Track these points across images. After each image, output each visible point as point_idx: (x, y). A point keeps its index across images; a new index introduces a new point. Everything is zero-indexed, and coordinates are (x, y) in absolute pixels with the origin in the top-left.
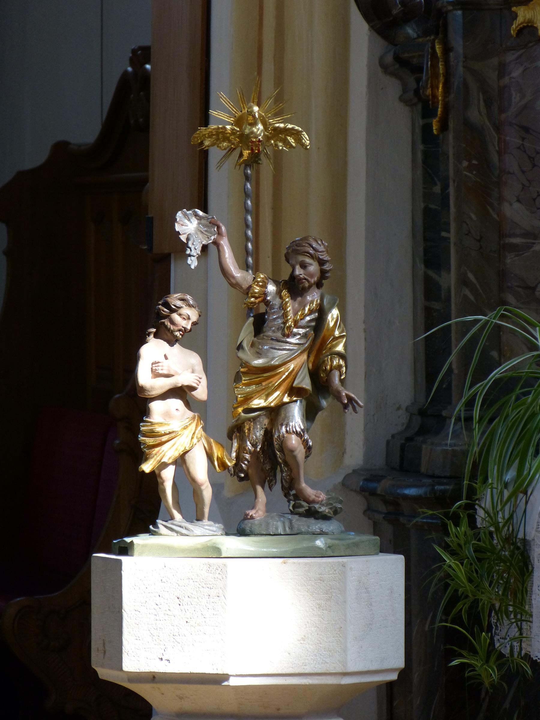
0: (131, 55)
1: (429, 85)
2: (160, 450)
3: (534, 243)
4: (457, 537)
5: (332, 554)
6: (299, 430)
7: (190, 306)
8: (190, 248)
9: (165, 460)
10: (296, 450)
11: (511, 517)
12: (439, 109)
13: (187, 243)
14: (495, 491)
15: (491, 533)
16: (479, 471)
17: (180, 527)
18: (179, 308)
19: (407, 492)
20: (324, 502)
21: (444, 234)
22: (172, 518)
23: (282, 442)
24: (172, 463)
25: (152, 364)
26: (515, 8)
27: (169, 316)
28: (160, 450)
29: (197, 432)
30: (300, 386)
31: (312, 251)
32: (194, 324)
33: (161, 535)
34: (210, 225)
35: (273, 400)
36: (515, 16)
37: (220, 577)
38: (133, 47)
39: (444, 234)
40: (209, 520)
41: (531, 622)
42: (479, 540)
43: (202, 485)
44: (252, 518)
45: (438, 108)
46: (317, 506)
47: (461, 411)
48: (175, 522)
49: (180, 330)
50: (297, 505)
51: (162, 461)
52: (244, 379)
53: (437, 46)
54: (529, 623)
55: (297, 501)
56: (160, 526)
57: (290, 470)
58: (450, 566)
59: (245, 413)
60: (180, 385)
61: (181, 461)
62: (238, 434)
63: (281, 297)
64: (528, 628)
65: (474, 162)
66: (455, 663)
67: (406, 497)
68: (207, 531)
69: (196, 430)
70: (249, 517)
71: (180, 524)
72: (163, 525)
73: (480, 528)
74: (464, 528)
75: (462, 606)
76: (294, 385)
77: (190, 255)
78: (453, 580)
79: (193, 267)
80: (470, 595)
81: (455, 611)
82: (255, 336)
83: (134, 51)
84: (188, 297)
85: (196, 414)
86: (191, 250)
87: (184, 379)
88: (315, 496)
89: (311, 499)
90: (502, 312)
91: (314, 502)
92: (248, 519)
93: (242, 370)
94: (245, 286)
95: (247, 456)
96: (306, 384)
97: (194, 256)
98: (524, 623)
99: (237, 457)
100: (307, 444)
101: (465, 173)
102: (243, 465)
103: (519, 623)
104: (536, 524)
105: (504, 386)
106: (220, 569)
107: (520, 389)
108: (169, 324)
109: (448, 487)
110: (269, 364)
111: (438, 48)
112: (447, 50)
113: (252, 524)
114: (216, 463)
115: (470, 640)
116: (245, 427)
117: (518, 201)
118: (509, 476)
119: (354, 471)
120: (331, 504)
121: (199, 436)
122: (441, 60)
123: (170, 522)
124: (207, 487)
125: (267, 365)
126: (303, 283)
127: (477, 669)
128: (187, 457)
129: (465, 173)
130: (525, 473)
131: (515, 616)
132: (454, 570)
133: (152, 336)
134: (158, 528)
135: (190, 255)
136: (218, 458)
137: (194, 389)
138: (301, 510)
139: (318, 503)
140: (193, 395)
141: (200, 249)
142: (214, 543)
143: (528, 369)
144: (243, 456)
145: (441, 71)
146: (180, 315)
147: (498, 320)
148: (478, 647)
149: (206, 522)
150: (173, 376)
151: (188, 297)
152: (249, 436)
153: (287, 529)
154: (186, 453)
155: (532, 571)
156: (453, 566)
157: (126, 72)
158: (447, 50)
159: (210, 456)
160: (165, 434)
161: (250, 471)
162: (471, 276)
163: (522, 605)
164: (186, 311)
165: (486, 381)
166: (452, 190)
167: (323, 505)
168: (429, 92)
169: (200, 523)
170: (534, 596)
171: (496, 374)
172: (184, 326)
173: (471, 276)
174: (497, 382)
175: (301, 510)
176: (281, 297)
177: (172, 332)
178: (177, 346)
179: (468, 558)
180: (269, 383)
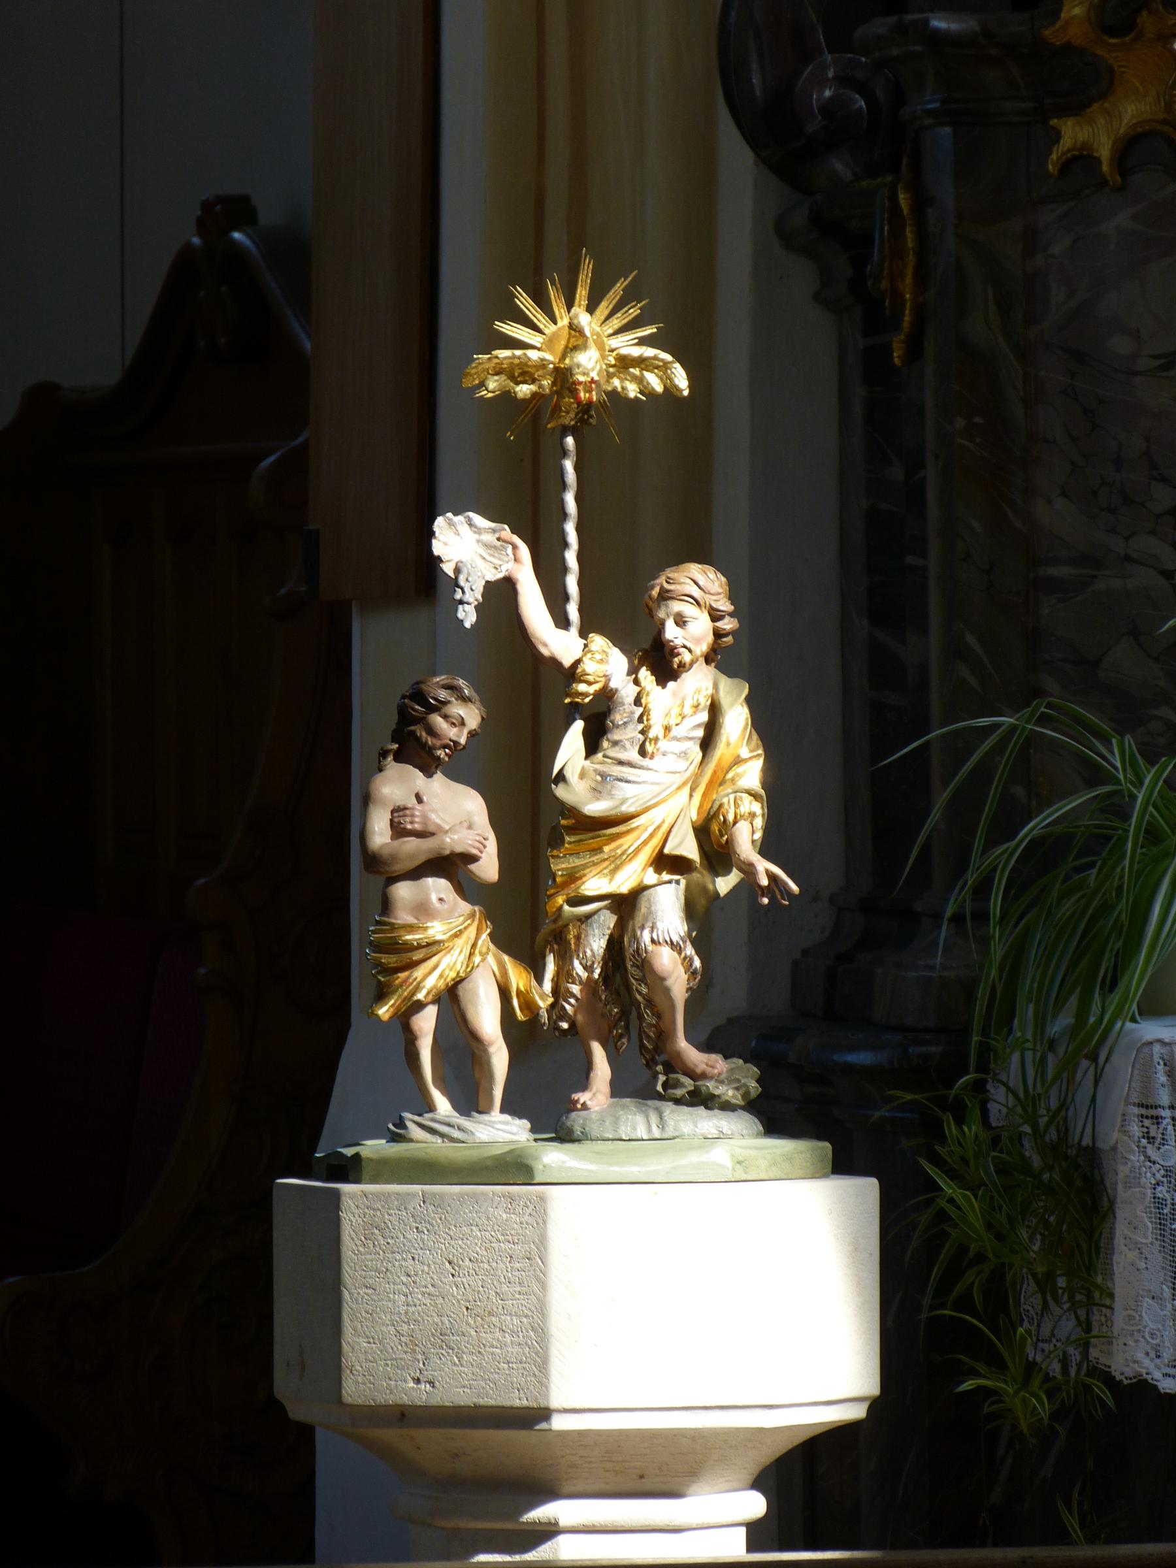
0: (199, 213)
1: (886, 272)
2: (408, 977)
3: (1095, 577)
4: (960, 1144)
5: (744, 1177)
6: (675, 939)
7: (464, 699)
8: (462, 589)
9: (420, 996)
10: (670, 976)
11: (1063, 1105)
12: (907, 318)
13: (457, 578)
14: (1029, 1055)
15: (1021, 1135)
16: (1004, 1015)
17: (449, 1125)
18: (445, 703)
19: (853, 1058)
20: (723, 1076)
21: (910, 559)
22: (430, 1107)
23: (644, 964)
24: (433, 1002)
25: (392, 812)
26: (1055, 121)
27: (424, 718)
28: (408, 977)
29: (480, 942)
30: (677, 852)
31: (696, 592)
32: (472, 735)
33: (411, 1141)
34: (499, 543)
35: (623, 883)
36: (1057, 136)
37: (531, 1220)
38: (204, 198)
39: (910, 559)
40: (502, 1111)
41: (1112, 1309)
42: (1001, 1151)
43: (491, 1044)
44: (585, 1107)
45: (903, 314)
46: (711, 1085)
47: (965, 901)
48: (438, 1117)
49: (445, 747)
50: (671, 1082)
51: (415, 998)
52: (567, 839)
53: (901, 196)
54: (1104, 1309)
55: (671, 1076)
56: (409, 1124)
57: (658, 1016)
58: (951, 1201)
59: (571, 906)
60: (447, 852)
61: (451, 998)
62: (556, 947)
63: (636, 682)
64: (1103, 1319)
65: (978, 420)
66: (967, 1385)
67: (850, 1069)
68: (500, 1133)
69: (477, 939)
70: (579, 1106)
71: (447, 1120)
72: (415, 1122)
73: (997, 1127)
74: (972, 1129)
75: (973, 1279)
76: (666, 851)
77: (461, 602)
78: (956, 1226)
79: (467, 625)
80: (991, 1256)
81: (959, 1288)
82: (587, 758)
83: (206, 206)
84: (461, 682)
85: (476, 908)
86: (463, 592)
87: (457, 840)
88: (707, 1065)
89: (698, 1071)
90: (1042, 709)
91: (704, 1076)
92: (577, 1110)
93: (563, 822)
94: (567, 662)
95: (576, 989)
96: (690, 849)
97: (468, 603)
98: (1095, 1309)
99: (556, 992)
100: (691, 965)
101: (959, 440)
102: (567, 1007)
103: (1082, 1313)
104: (1119, 1118)
105: (1044, 856)
106: (532, 1207)
107: (1075, 859)
108: (424, 734)
109: (934, 1049)
110: (617, 810)
111: (904, 200)
112: (921, 202)
113: (585, 1120)
114: (515, 1002)
115: (990, 1340)
116: (569, 932)
117: (1064, 494)
118: (1060, 1024)
119: (731, 1021)
120: (738, 1080)
121: (484, 950)
122: (908, 222)
123: (427, 1115)
124: (500, 1047)
125: (613, 812)
126: (678, 654)
127: (1007, 1399)
128: (461, 990)
129: (959, 440)
130: (1092, 1020)
131: (1071, 1297)
132: (959, 1208)
133: (390, 758)
134: (405, 1127)
135: (461, 602)
136: (519, 992)
137: (474, 859)
138: (679, 1092)
139: (712, 1078)
140: (471, 872)
141: (481, 589)
142: (519, 1156)
143: (1090, 819)
144: (567, 990)
145: (910, 245)
146: (445, 717)
147: (1035, 725)
148: (1006, 1356)
149: (496, 1115)
150: (433, 834)
151: (461, 682)
152: (577, 950)
153: (654, 1128)
154: (458, 982)
155: (1112, 1209)
156: (960, 1201)
157: (188, 246)
158: (921, 202)
159: (504, 993)
160: (420, 947)
161: (579, 1018)
162: (971, 640)
163: (1090, 1275)
164: (458, 709)
165: (1014, 843)
166: (931, 473)
167: (722, 1082)
168: (885, 284)
169: (485, 1117)
170: (1116, 1258)
171: (1033, 828)
172: (454, 738)
173: (971, 640)
174: (1035, 844)
175: (679, 1092)
176: (636, 682)
177: (430, 751)
178: (439, 776)
179: (986, 1185)
180: (618, 848)
